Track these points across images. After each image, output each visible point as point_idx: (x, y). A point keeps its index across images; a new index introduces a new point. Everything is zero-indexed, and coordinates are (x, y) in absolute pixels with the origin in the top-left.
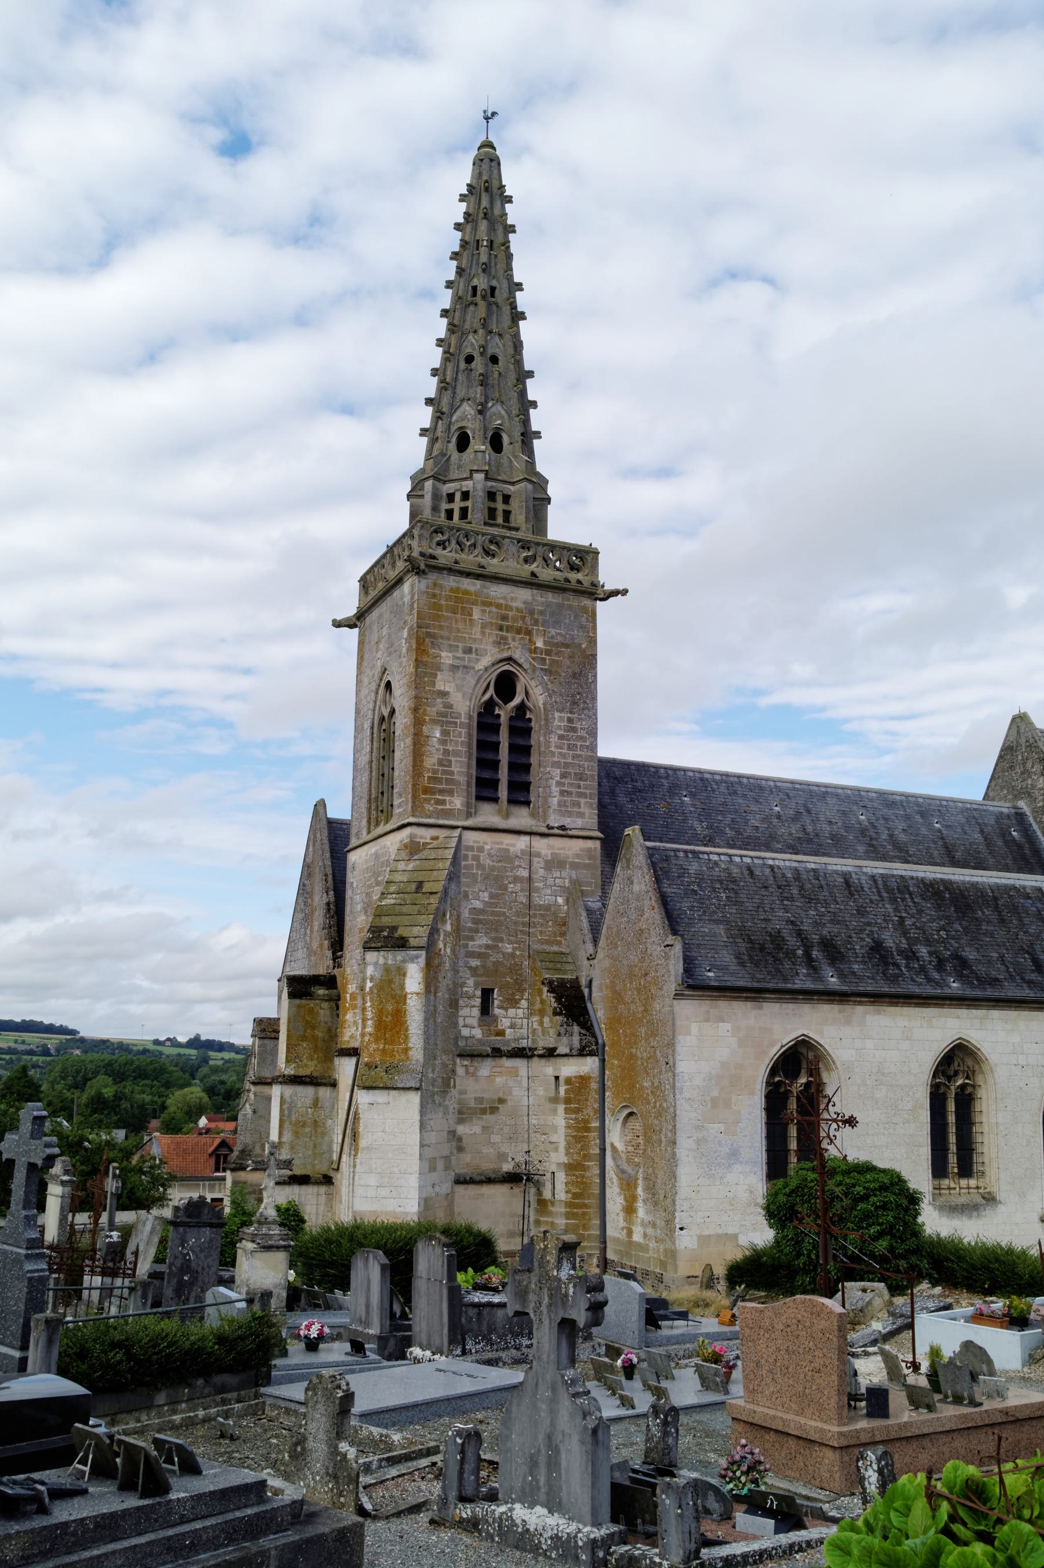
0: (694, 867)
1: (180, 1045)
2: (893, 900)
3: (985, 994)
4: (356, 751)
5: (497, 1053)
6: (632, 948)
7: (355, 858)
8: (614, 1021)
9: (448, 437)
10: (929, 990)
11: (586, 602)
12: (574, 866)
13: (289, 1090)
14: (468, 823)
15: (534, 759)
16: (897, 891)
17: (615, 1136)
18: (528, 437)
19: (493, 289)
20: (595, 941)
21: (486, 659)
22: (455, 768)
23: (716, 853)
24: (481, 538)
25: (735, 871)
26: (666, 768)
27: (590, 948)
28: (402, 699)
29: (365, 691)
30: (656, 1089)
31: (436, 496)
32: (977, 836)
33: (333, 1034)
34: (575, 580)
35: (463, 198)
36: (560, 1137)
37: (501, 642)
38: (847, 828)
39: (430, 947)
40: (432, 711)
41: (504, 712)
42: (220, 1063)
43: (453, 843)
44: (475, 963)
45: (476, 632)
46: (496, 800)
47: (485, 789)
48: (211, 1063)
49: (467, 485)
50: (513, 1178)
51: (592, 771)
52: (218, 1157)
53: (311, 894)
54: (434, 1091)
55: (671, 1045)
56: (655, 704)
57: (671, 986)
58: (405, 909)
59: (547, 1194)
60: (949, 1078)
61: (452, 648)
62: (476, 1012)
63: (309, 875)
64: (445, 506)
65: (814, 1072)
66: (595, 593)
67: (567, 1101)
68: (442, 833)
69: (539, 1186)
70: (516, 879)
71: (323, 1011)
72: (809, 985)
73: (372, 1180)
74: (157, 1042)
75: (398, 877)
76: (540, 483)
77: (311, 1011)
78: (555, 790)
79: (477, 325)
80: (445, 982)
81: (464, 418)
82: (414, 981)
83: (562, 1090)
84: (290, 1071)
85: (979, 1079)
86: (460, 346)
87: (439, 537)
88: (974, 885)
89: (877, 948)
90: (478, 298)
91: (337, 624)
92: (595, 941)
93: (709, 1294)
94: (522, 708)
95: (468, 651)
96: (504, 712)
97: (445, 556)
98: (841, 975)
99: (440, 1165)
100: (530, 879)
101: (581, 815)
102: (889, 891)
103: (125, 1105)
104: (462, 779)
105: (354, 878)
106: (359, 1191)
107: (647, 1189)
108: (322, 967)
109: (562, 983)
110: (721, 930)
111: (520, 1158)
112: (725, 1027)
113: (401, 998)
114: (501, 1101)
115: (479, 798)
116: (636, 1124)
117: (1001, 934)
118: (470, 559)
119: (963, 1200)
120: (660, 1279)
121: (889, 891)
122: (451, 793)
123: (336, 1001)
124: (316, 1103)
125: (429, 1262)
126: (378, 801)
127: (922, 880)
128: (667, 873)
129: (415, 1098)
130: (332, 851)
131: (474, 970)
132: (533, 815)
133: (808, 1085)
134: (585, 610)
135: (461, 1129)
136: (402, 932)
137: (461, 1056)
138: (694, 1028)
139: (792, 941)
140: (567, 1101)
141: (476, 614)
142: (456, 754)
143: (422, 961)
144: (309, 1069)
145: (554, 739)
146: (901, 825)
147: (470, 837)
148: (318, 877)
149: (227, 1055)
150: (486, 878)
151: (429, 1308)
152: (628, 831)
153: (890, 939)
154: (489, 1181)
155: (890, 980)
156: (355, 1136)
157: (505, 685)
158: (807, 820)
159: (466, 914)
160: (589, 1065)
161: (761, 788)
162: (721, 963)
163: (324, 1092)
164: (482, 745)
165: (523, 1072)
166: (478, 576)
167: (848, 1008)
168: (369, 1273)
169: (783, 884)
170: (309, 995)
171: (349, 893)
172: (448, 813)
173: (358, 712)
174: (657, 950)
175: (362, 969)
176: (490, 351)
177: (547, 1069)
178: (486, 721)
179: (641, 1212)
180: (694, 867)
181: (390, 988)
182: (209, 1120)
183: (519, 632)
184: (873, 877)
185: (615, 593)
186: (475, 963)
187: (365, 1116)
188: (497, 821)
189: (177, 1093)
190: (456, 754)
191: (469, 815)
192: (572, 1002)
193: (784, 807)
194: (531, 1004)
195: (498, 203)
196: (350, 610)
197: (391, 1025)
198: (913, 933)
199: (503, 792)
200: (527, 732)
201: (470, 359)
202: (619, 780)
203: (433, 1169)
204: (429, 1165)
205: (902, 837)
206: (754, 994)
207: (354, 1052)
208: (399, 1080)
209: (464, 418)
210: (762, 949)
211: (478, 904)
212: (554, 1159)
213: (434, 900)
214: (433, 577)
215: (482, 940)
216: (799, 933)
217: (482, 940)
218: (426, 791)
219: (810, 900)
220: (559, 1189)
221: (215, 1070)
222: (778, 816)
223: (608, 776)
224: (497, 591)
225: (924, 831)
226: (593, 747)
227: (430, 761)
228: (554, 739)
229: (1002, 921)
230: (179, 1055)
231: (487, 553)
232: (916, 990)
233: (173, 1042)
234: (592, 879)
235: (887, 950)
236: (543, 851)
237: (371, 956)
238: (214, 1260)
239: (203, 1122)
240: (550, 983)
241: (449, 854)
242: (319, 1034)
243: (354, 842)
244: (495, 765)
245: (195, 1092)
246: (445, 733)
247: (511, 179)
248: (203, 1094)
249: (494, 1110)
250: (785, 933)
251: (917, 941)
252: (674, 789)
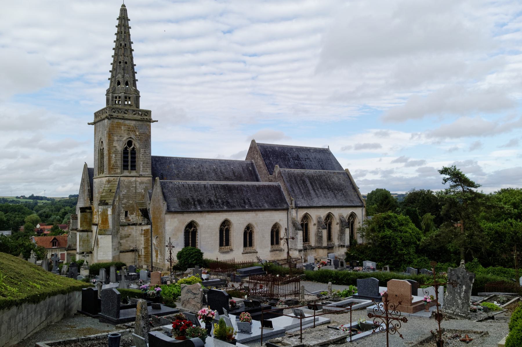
0: (171, 185)
1: (26, 198)
2: (214, 190)
3: (232, 209)
4: (95, 155)
5: (129, 225)
6: (157, 204)
8: (154, 218)
9: (115, 81)
10: (220, 209)
11: (148, 123)
12: (146, 183)
13: (81, 233)
15: (136, 160)
16: (215, 187)
17: (154, 241)
18: (135, 81)
19: (125, 44)
20: (150, 200)
21: (125, 138)
22: (118, 163)
24: (123, 110)
26: (169, 157)
28: (105, 146)
29: (96, 142)
30: (162, 232)
31: (113, 97)
32: (241, 169)
33: (91, 220)
34: (146, 118)
36: (143, 242)
37: (128, 134)
38: (210, 169)
39: (113, 205)
40: (112, 151)
41: (129, 149)
42: (42, 204)
43: (118, 180)
44: (123, 206)
45: (123, 132)
46: (128, 169)
47: (125, 167)
48: (39, 204)
49: (120, 95)
50: (132, 251)
52: (53, 243)
53: (84, 186)
54: (115, 234)
55: (164, 224)
57: (164, 212)
59: (140, 254)
61: (117, 136)
62: (124, 216)
63: (84, 181)
64: (115, 99)
65: (195, 227)
66: (150, 121)
67: (144, 234)
68: (115, 178)
69: (138, 252)
70: (133, 187)
71: (89, 215)
72: (194, 210)
73: (102, 253)
74: (17, 197)
75: (106, 189)
76: (137, 92)
77: (86, 215)
78: (141, 167)
79: (122, 54)
80: (117, 211)
81: (119, 78)
82: (110, 212)
83: (143, 232)
84: (81, 229)
85: (230, 226)
86: (117, 60)
87: (113, 110)
88: (233, 185)
89: (210, 202)
90: (122, 47)
91: (89, 124)
92: (150, 200)
94: (134, 148)
95: (121, 136)
96: (129, 149)
97: (115, 115)
98: (201, 207)
99: (116, 249)
101: (147, 172)
102: (214, 188)
103: (11, 222)
104: (120, 166)
105: (95, 185)
106: (99, 256)
107: (160, 252)
108: (88, 205)
109: (143, 209)
111: (134, 247)
112: (176, 219)
115: (124, 169)
116: (158, 239)
117: (238, 196)
118: (121, 115)
119: (226, 251)
121: (214, 188)
122: (117, 169)
123: (92, 213)
124: (88, 236)
125: (112, 270)
126: (101, 169)
128: (165, 187)
129: (111, 236)
130: (89, 176)
131: (123, 207)
132: (136, 172)
133: (194, 230)
134: (148, 125)
135: (121, 241)
136: (107, 201)
137: (121, 226)
138: (169, 220)
139: (191, 200)
140: (144, 234)
141: (122, 128)
142: (118, 160)
143: (111, 208)
144: (86, 228)
145: (141, 155)
146: (223, 168)
147: (122, 178)
148: (86, 182)
149: (44, 201)
150: (126, 187)
152: (156, 178)
153: (213, 199)
154: (127, 252)
155: (211, 207)
156: (98, 244)
157: (130, 143)
158: (201, 168)
159: (121, 195)
160: (149, 227)
161: (191, 161)
162: (176, 206)
163: (89, 233)
164: (124, 157)
166: (123, 119)
167: (202, 214)
168: (102, 272)
169: (190, 188)
170: (85, 212)
171: (94, 188)
172: (117, 174)
173: (95, 146)
175: (97, 209)
176: (125, 61)
177: (140, 228)
178: (125, 151)
179: (159, 257)
180: (171, 185)
181: (104, 215)
182: (41, 225)
184: (211, 185)
185: (155, 121)
186: (123, 206)
188: (128, 174)
189: (28, 217)
190: (118, 160)
191: (122, 173)
192: (145, 213)
194: (136, 214)
195: (126, 22)
196: (92, 121)
197: (105, 221)
198: (218, 197)
199: (129, 168)
201: (120, 62)
202: (157, 161)
203: (115, 250)
204: (114, 249)
205: (223, 171)
206: (182, 212)
207: (96, 225)
208: (107, 233)
209: (119, 78)
210: (184, 203)
211: (124, 193)
212: (141, 246)
213: (114, 194)
214: (112, 120)
215: (125, 201)
217: (125, 201)
218: (112, 169)
219: (196, 191)
220: (143, 252)
221: (41, 207)
222: (195, 168)
223: (155, 160)
224: (127, 122)
225: (229, 169)
227: (112, 162)
228: (141, 155)
229: (238, 193)
230: (26, 202)
231: (125, 113)
232: (217, 209)
233: (24, 197)
234: (150, 186)
235: (212, 201)
236: (140, 180)
237: (100, 207)
238: (77, 271)
239: (38, 226)
241: (117, 183)
243: (95, 177)
244: (128, 161)
245: (35, 216)
246: (116, 155)
247: (130, 14)
248: (38, 217)
249: (128, 237)
250: (190, 199)
252: (170, 163)
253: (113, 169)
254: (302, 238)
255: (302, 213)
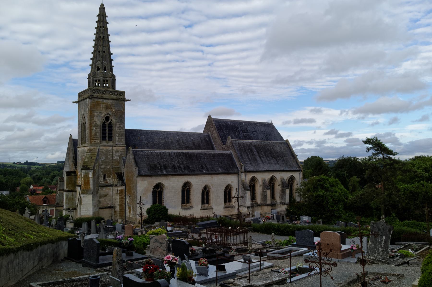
2: (177, 157)
3: (192, 173)
5: (107, 186)
6: (130, 168)
7: (79, 149)
9: (95, 67)
10: (182, 173)
11: (123, 102)
12: (121, 151)
13: (67, 193)
14: (101, 145)
15: (113, 132)
16: (178, 155)
17: (128, 200)
18: (112, 67)
19: (104, 37)
20: (124, 165)
21: (103, 114)
23: (146, 150)
25: (149, 153)
27: (123, 167)
28: (87, 121)
29: (80, 117)
31: (93, 80)
32: (200, 140)
33: (75, 182)
34: (121, 97)
35: (97, 16)
36: (118, 200)
37: (106, 111)
39: (94, 169)
40: (93, 125)
41: (107, 123)
44: (102, 170)
46: (106, 140)
47: (103, 138)
48: (32, 169)
49: (99, 78)
50: (110, 207)
51: (124, 133)
53: (70, 154)
54: (95, 194)
55: (136, 185)
56: (136, 118)
57: (136, 175)
58: (89, 162)
59: (116, 210)
60: (186, 187)
61: (97, 112)
62: (103, 179)
64: (95, 82)
65: (161, 188)
67: (119, 194)
68: (96, 147)
69: (114, 208)
70: (110, 155)
71: (73, 178)
72: (160, 174)
73: (84, 209)
74: (14, 163)
75: (87, 156)
76: (114, 76)
78: (117, 138)
80: (96, 175)
81: (98, 64)
82: (91, 175)
88: (193, 153)
89: (174, 167)
90: (101, 39)
91: (74, 102)
93: (139, 225)
94: (111, 123)
95: (100, 113)
96: (107, 123)
97: (95, 95)
98: (166, 172)
99: (96, 206)
100: (112, 154)
101: (122, 142)
102: (177, 155)
103: (9, 184)
104: (99, 137)
105: (79, 153)
106: (82, 211)
108: (73, 169)
109: (118, 173)
110: (145, 164)
111: (111, 204)
113: (89, 178)
114: (108, 194)
115: (102, 140)
116: (131, 198)
120: (134, 223)
121: (177, 155)
122: (97, 140)
123: (76, 176)
124: (72, 195)
125: (93, 223)
126: (83, 139)
127: (183, 153)
129: (92, 196)
130: (74, 145)
131: (102, 172)
132: (113, 142)
134: (123, 103)
135: (100, 200)
136: (88, 167)
137: (100, 187)
138: (140, 182)
139: (158, 166)
140: (119, 194)
142: (98, 132)
143: (92, 172)
144: (71, 188)
145: (117, 128)
146: (184, 139)
147: (101, 148)
149: (36, 167)
151: (93, 228)
153: (176, 164)
154: (105, 208)
155: (175, 172)
157: (107, 118)
158: (166, 139)
159: (100, 161)
160: (123, 188)
161: (158, 133)
162: (145, 170)
163: (74, 193)
165: (112, 189)
166: (102, 98)
167: (167, 177)
168: (85, 225)
169: (157, 155)
171: (78, 156)
172: (97, 143)
174: (134, 169)
175: (81, 173)
176: (104, 50)
177: (116, 188)
180: (141, 153)
181: (86, 177)
182: (34, 186)
183: (110, 108)
184: (174, 153)
185: (128, 100)
186: (102, 170)
187: (83, 199)
188: (106, 144)
189: (23, 179)
190: (98, 132)
191: (101, 143)
192: (120, 176)
193: (162, 137)
194: (113, 177)
196: (77, 100)
197: (87, 182)
198: (181, 163)
199: (107, 139)
200: (112, 127)
201: (99, 52)
204: (94, 206)
205: (185, 141)
206: (151, 176)
209: (98, 64)
211: (103, 160)
213: (94, 160)
214: (93, 99)
215: (103, 166)
216: (160, 164)
217: (103, 166)
220: (118, 209)
221: (34, 171)
222: (161, 139)
224: (105, 101)
225: (189, 140)
226: (124, 127)
227: (93, 134)
228: (117, 128)
229: (197, 160)
230: (22, 167)
231: (103, 94)
232: (179, 173)
233: (20, 163)
236: (115, 149)
237: (83, 171)
239: (32, 187)
240: (116, 173)
241: (97, 151)
242: (73, 182)
243: (78, 146)
244: (106, 134)
246: (96, 129)
248: (31, 179)
249: (106, 196)
251: (181, 164)
252: (141, 135)
253: (93, 140)
254: (250, 197)
255: (250, 176)
